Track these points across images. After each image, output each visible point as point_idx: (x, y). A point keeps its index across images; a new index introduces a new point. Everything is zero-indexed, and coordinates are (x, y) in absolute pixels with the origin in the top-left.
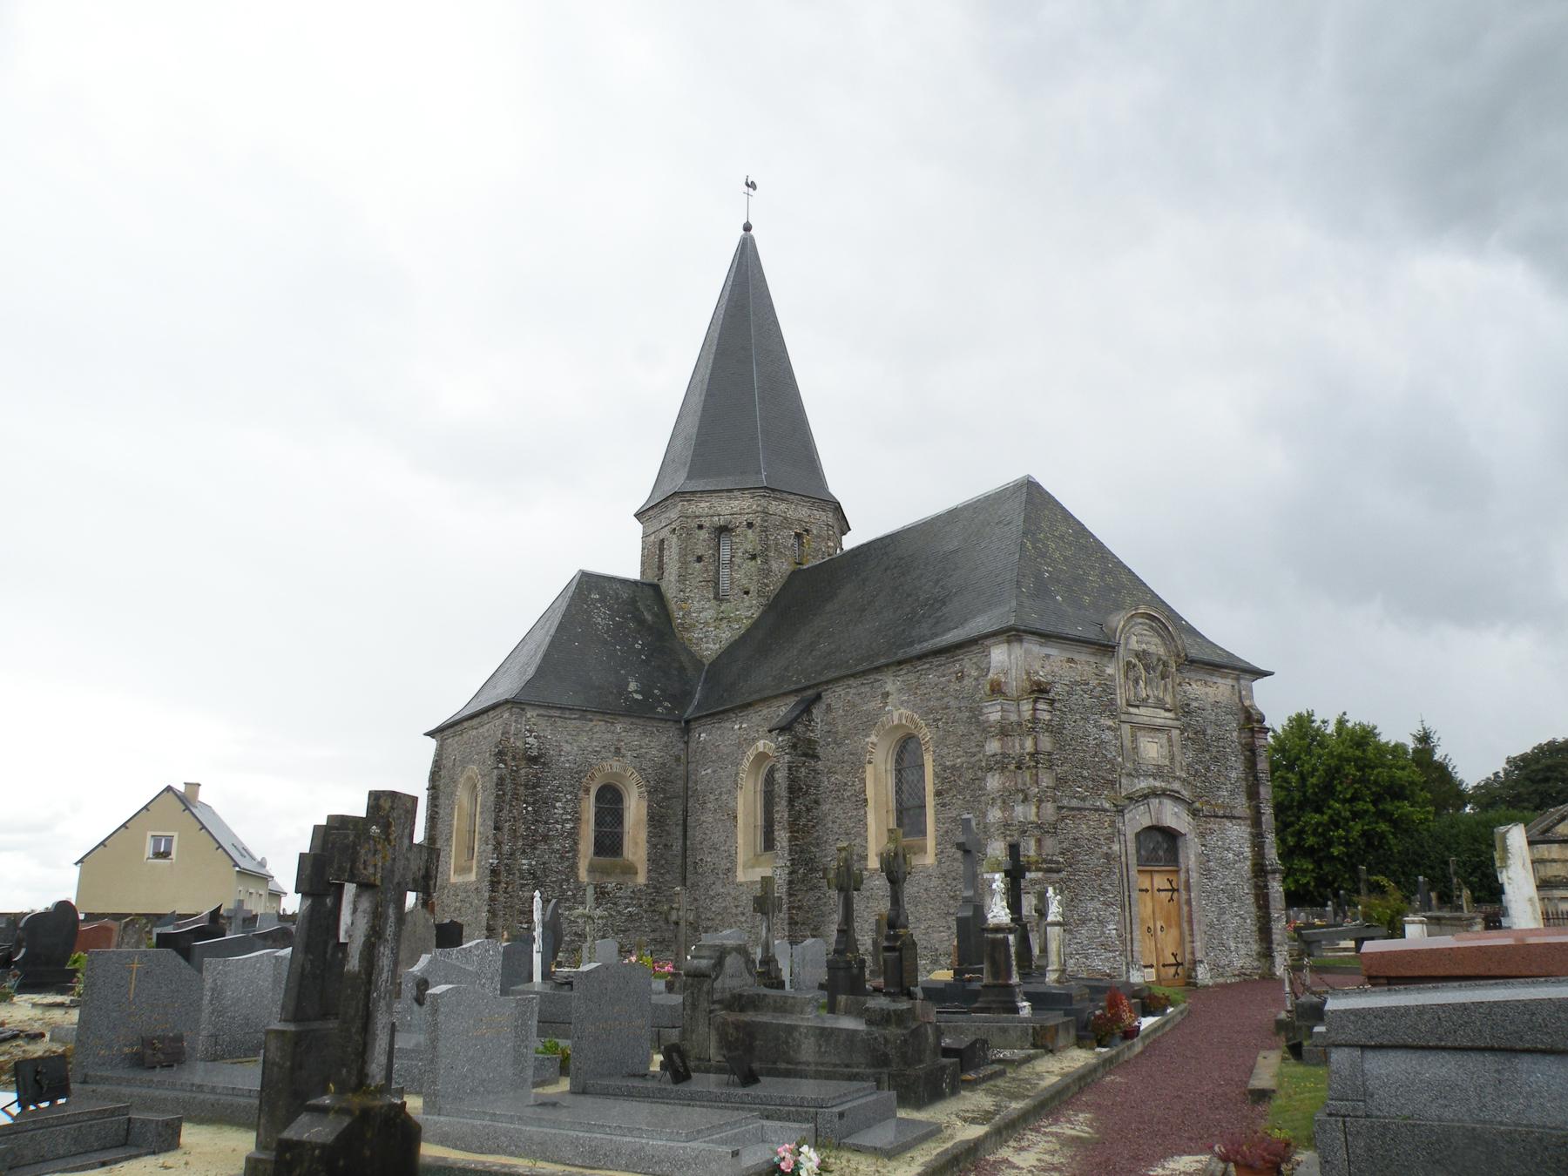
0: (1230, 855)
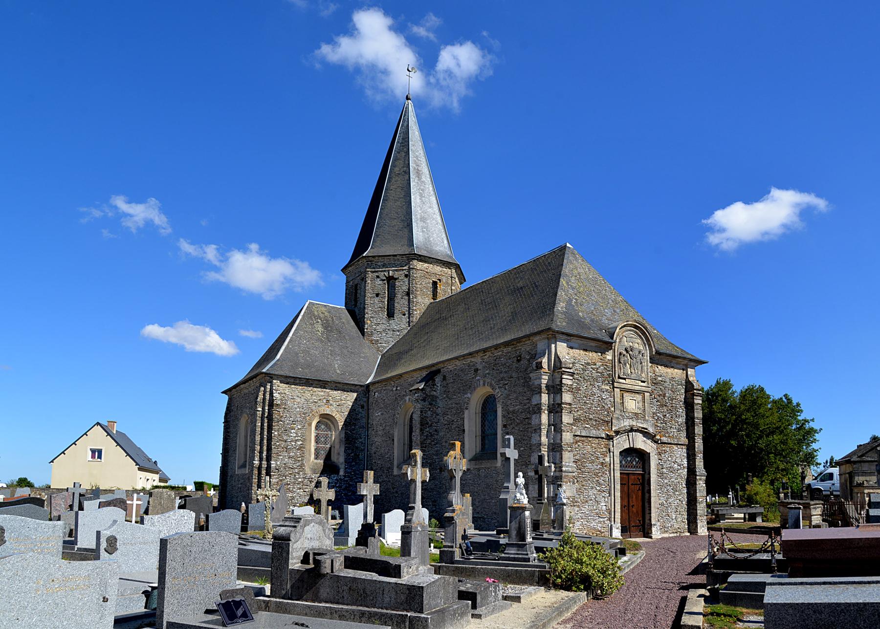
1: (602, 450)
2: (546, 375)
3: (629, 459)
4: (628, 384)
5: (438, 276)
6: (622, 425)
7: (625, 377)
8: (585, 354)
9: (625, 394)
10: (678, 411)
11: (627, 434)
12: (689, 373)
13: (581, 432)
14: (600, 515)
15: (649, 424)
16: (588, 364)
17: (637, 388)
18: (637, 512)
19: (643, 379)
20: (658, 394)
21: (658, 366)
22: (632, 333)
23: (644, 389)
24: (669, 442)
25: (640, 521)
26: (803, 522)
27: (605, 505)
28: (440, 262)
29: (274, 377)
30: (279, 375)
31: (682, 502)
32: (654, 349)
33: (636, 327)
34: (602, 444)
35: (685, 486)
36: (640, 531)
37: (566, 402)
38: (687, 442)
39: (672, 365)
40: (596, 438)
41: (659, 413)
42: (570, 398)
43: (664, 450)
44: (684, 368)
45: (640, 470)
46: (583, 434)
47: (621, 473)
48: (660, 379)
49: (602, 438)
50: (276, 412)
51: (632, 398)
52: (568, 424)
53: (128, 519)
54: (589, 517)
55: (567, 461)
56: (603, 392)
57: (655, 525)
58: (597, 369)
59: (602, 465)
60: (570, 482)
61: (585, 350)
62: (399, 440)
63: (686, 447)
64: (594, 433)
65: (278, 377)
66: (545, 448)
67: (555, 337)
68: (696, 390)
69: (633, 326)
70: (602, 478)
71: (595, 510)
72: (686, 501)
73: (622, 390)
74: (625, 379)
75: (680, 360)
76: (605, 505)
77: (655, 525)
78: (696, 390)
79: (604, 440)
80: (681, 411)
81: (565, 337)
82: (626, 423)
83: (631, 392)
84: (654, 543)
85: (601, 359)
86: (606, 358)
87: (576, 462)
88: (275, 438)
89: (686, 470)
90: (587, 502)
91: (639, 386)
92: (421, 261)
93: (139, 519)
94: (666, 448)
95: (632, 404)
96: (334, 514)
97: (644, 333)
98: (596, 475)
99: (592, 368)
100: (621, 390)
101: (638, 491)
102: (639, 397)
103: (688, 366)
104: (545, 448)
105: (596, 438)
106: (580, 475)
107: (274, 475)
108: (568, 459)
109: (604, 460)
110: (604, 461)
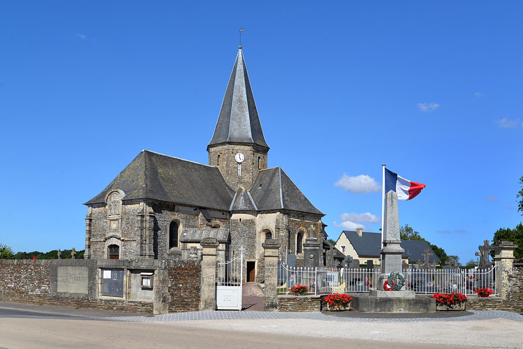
0: (132, 251)
3: (116, 249)
4: (112, 217)
5: (220, 152)
6: (109, 235)
9: (111, 222)
15: (120, 233)
16: (100, 213)
17: (115, 218)
19: (118, 214)
23: (118, 218)
24: (129, 240)
26: (466, 290)
28: (219, 144)
39: (134, 203)
40: (100, 242)
46: (95, 241)
48: (127, 211)
53: (289, 286)
61: (99, 207)
62: (294, 238)
64: (99, 240)
73: (111, 220)
82: (111, 234)
89: (322, 245)
91: (116, 217)
92: (213, 147)
93: (310, 286)
94: (128, 243)
95: (114, 225)
96: (236, 279)
102: (117, 222)
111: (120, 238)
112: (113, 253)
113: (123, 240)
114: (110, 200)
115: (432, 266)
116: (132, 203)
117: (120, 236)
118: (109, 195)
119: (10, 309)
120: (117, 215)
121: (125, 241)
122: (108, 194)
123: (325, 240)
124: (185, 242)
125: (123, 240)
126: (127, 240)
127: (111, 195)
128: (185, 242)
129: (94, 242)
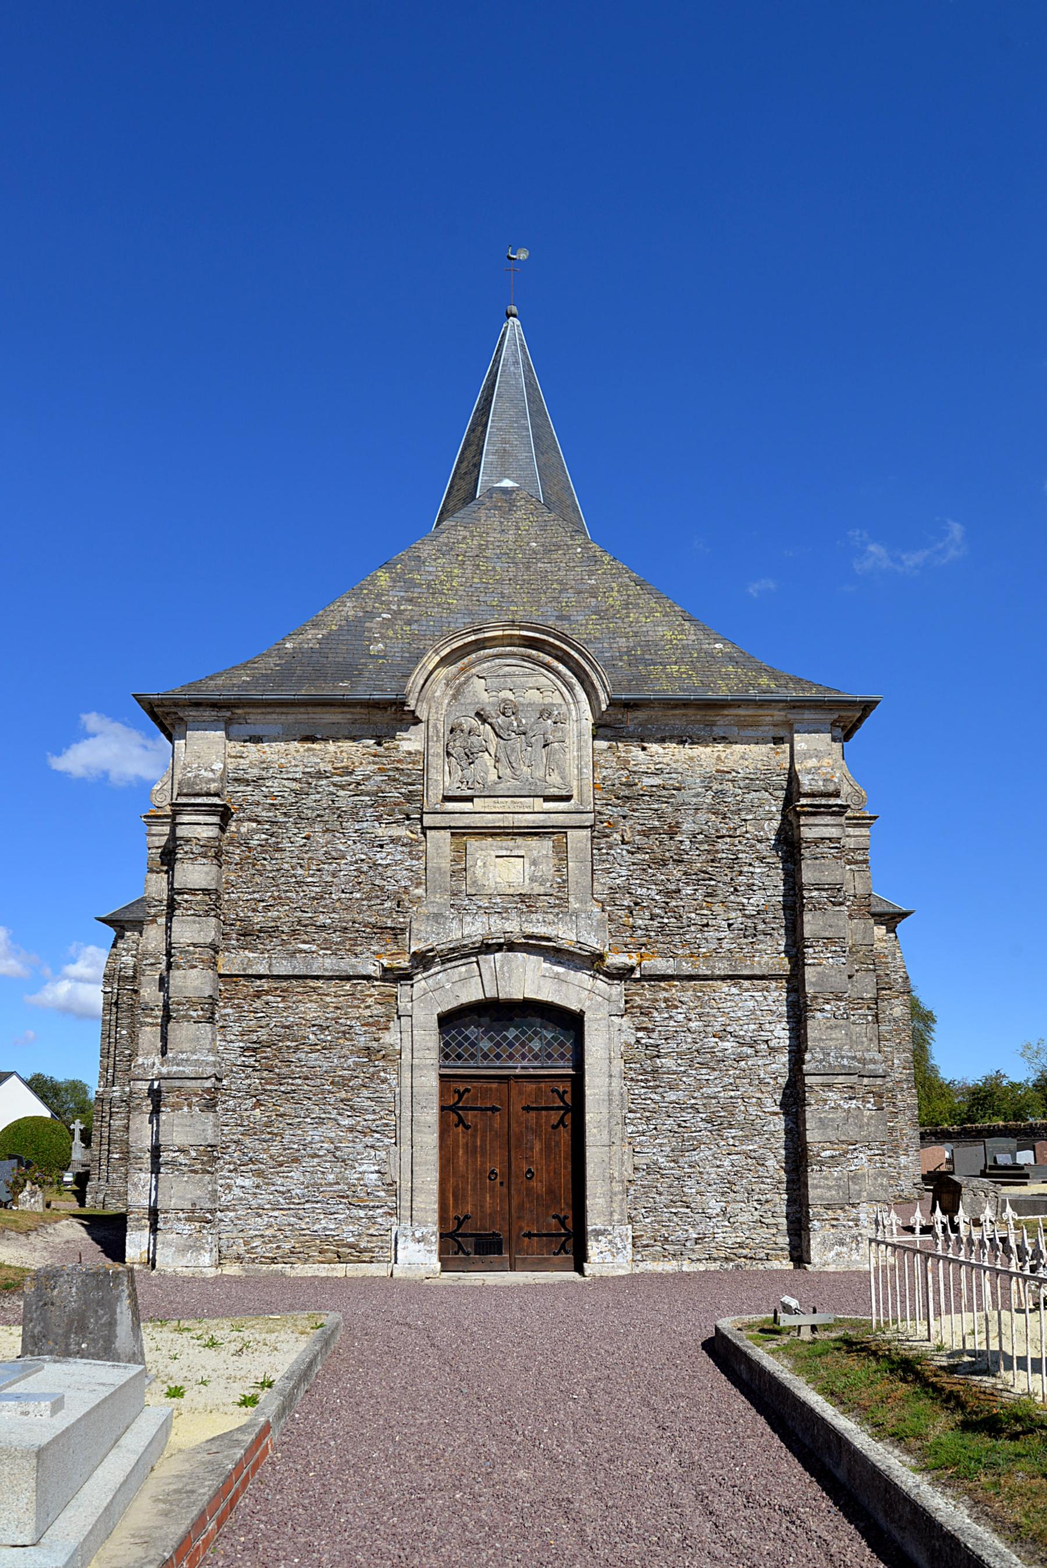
1: (367, 1012)
2: (163, 824)
7: (469, 793)
8: (309, 749)
9: (473, 843)
10: (741, 872)
11: (474, 959)
12: (797, 747)
13: (270, 965)
14: (354, 1201)
16: (320, 775)
18: (550, 1191)
20: (639, 828)
21: (646, 745)
22: (514, 662)
25: (562, 1222)
27: (378, 1172)
29: (126, 926)
30: (136, 921)
31: (761, 1162)
32: (603, 696)
33: (510, 641)
34: (371, 996)
35: (777, 1109)
36: (563, 1248)
37: (189, 887)
38: (788, 967)
39: (718, 731)
41: (641, 886)
42: (207, 873)
43: (666, 1000)
44: (781, 734)
45: (561, 1063)
47: (441, 1076)
49: (368, 978)
50: (125, 992)
51: (504, 853)
52: (194, 945)
54: (307, 1206)
55: (186, 1046)
56: (382, 846)
57: (598, 1233)
58: (359, 784)
59: (368, 1056)
60: (190, 1106)
63: (785, 984)
65: (134, 924)
66: (156, 1017)
67: (181, 719)
68: (807, 795)
69: (517, 642)
70: (365, 1093)
71: (331, 1184)
72: (781, 1158)
73: (459, 833)
74: (469, 799)
75: (741, 712)
76: (378, 1172)
77: (598, 1233)
78: (807, 795)
79: (376, 983)
80: (758, 870)
81: (208, 714)
83: (508, 834)
84: (584, 1286)
85: (375, 756)
86: (396, 748)
87: (254, 1050)
88: (122, 1041)
90: (296, 1160)
97: (564, 658)
98: (342, 1083)
99: (335, 785)
100: (453, 834)
101: (554, 1127)
102: (544, 847)
103: (796, 727)
104: (156, 1017)
105: (341, 978)
106: (268, 1087)
107: (117, 1113)
108: (191, 1040)
109: (376, 1040)
110: (375, 1044)
111: (601, 957)
112: (452, 1063)
113: (623, 974)
114: (454, 697)
115: (486, 1198)
116: (698, 730)
117: (594, 942)
118: (444, 662)
119: (812, 1410)
120: (547, 799)
121: (644, 978)
122: (437, 652)
123: (669, 900)
124: (477, 962)
125: (623, 974)
126: (670, 972)
127: (472, 665)
128: (477, 962)
129: (260, 977)
